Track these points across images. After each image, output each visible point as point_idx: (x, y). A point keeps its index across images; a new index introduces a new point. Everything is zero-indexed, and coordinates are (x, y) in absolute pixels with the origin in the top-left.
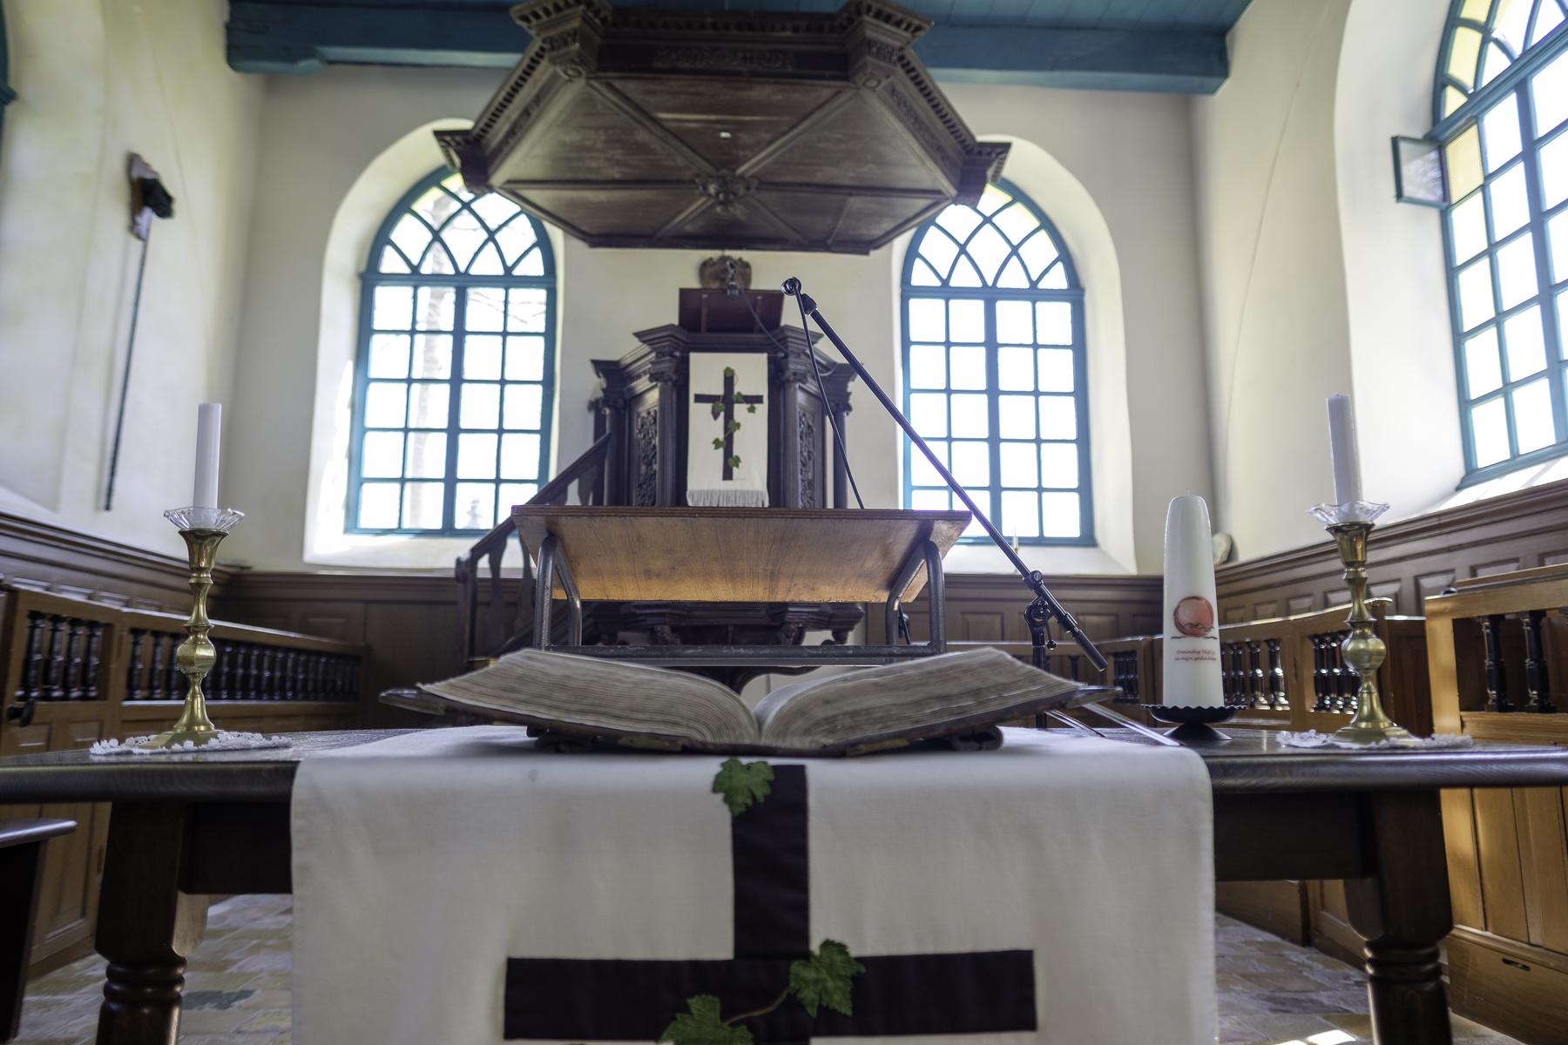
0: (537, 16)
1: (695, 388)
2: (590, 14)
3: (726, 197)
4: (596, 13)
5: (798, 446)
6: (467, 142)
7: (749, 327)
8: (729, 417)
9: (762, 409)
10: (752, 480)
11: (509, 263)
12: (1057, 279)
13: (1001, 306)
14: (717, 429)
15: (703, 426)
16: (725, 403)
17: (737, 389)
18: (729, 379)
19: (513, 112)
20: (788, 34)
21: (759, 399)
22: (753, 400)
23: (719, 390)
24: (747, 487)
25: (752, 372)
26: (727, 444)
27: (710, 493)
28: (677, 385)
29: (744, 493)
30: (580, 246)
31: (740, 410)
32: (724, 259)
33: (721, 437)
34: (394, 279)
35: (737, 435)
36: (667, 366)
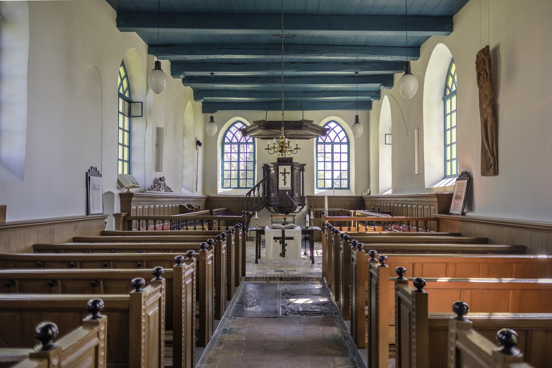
1: (280, 172)
5: (295, 178)
9: (290, 174)
10: (288, 186)
12: (345, 140)
13: (335, 146)
14: (283, 178)
15: (281, 177)
16: (284, 174)
18: (285, 170)
25: (288, 169)
26: (285, 180)
28: (277, 170)
31: (287, 175)
34: (227, 143)
36: (275, 168)
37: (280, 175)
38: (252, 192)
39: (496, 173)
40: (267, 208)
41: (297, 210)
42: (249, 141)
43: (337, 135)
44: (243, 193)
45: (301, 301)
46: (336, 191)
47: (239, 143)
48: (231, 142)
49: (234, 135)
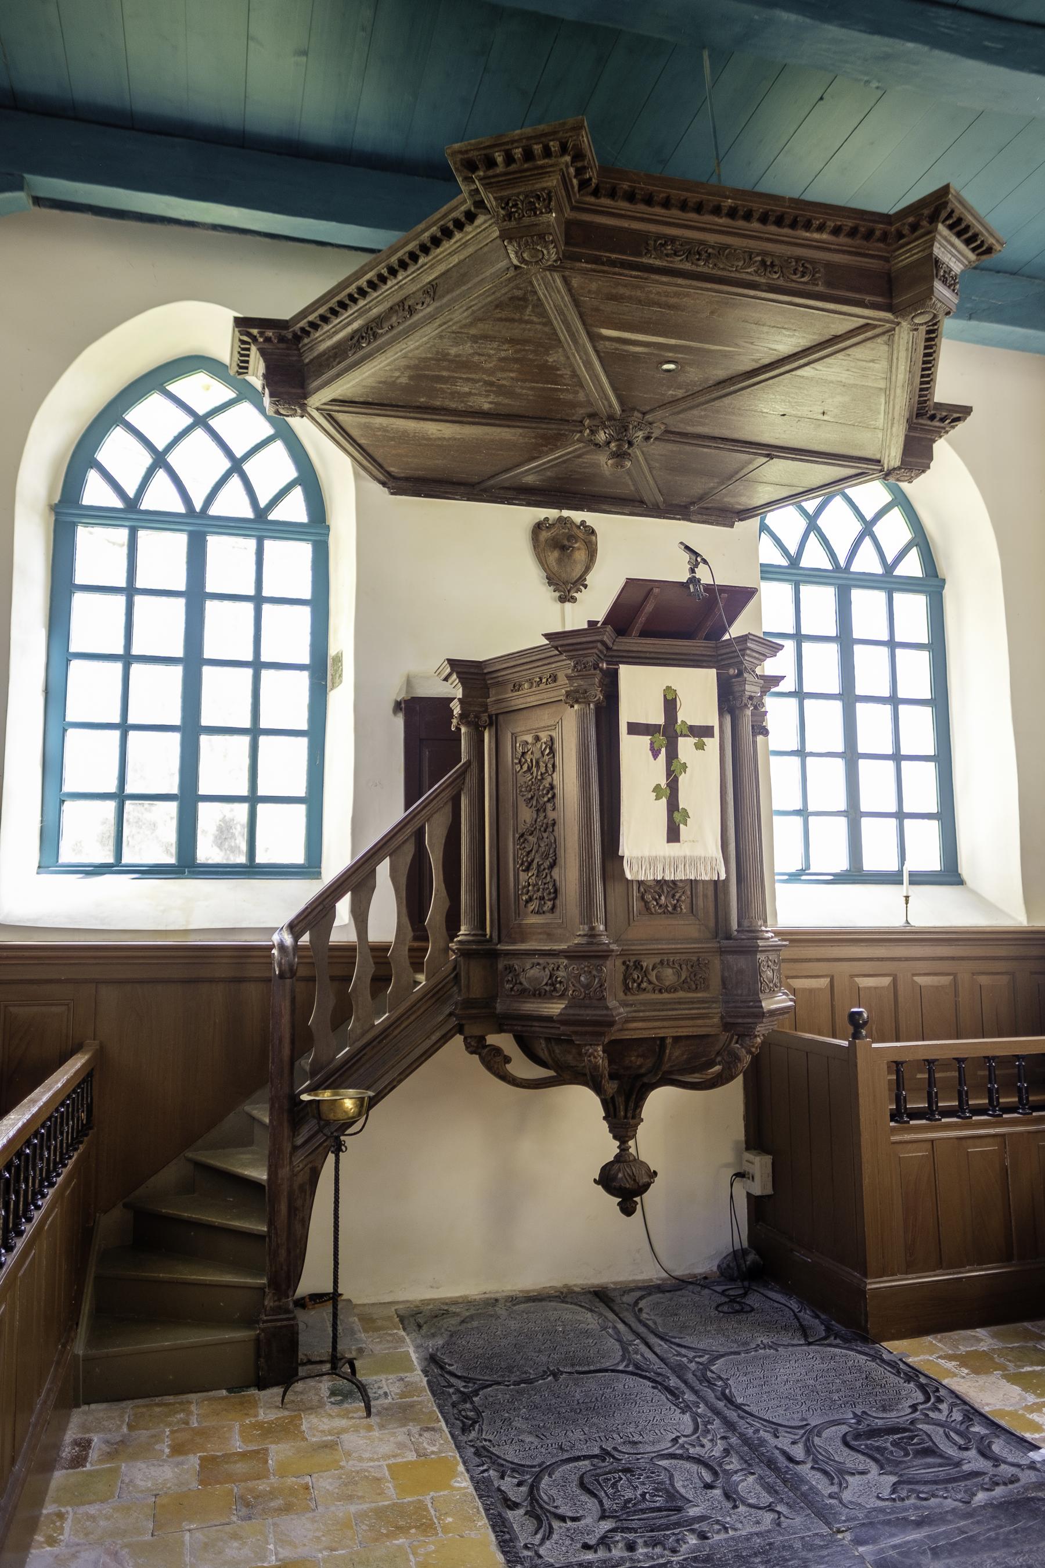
0: (491, 163)
1: (626, 716)
2: (572, 170)
3: (619, 447)
4: (579, 171)
6: (282, 339)
8: (672, 755)
11: (263, 503)
12: (912, 567)
14: (657, 771)
15: (639, 766)
16: (666, 734)
17: (681, 717)
18: (670, 705)
19: (377, 304)
20: (825, 236)
21: (707, 731)
22: (702, 732)
23: (657, 718)
24: (699, 852)
25: (697, 690)
26: (671, 792)
27: (652, 861)
29: (693, 862)
30: (378, 492)
31: (686, 745)
32: (561, 519)
33: (663, 783)
34: (102, 516)
35: (682, 779)
37: (633, 751)
38: (343, 907)
39: (678, 841)
40: (477, 1046)
42: (900, 571)
44: (265, 912)
47: (198, 525)
48: (261, 513)
49: (160, 460)
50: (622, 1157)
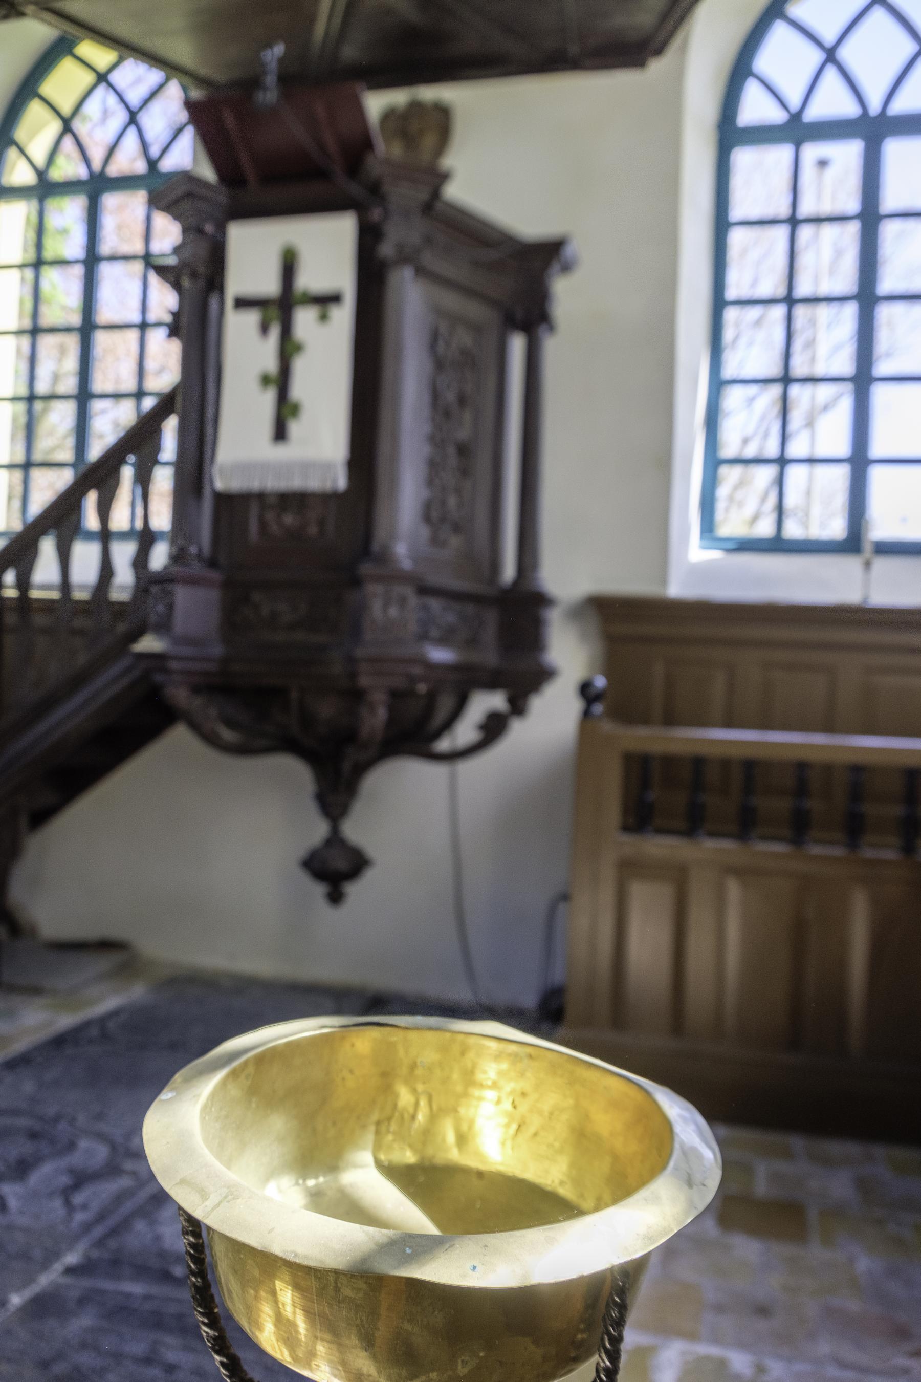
7: (321, 174)
9: (343, 317)
10: (321, 446)
14: (265, 353)
16: (280, 309)
18: (289, 266)
21: (336, 298)
26: (281, 381)
29: (306, 467)
31: (305, 320)
34: (762, 135)
41: (465, 732)
43: (133, 118)
45: (192, 1265)
46: (882, 565)
50: (335, 840)
